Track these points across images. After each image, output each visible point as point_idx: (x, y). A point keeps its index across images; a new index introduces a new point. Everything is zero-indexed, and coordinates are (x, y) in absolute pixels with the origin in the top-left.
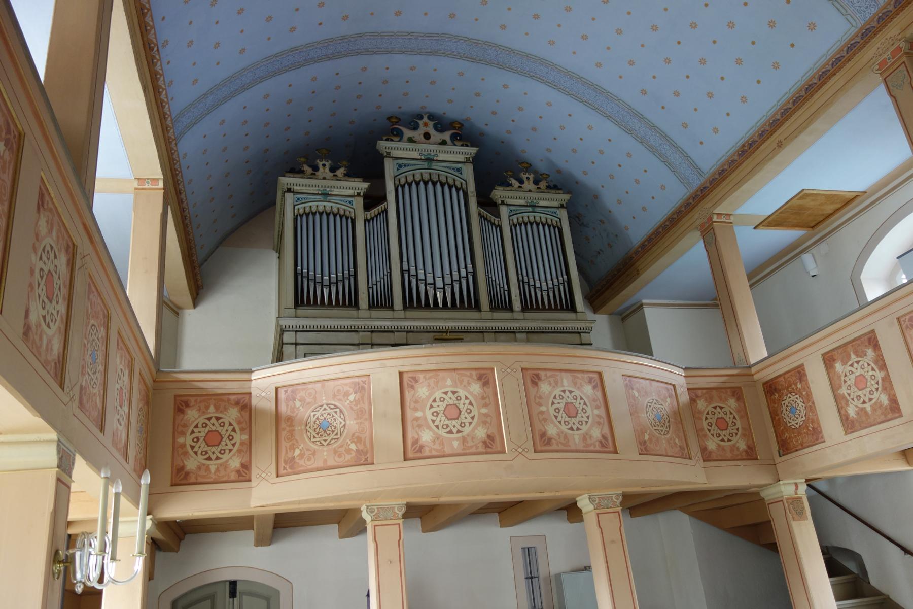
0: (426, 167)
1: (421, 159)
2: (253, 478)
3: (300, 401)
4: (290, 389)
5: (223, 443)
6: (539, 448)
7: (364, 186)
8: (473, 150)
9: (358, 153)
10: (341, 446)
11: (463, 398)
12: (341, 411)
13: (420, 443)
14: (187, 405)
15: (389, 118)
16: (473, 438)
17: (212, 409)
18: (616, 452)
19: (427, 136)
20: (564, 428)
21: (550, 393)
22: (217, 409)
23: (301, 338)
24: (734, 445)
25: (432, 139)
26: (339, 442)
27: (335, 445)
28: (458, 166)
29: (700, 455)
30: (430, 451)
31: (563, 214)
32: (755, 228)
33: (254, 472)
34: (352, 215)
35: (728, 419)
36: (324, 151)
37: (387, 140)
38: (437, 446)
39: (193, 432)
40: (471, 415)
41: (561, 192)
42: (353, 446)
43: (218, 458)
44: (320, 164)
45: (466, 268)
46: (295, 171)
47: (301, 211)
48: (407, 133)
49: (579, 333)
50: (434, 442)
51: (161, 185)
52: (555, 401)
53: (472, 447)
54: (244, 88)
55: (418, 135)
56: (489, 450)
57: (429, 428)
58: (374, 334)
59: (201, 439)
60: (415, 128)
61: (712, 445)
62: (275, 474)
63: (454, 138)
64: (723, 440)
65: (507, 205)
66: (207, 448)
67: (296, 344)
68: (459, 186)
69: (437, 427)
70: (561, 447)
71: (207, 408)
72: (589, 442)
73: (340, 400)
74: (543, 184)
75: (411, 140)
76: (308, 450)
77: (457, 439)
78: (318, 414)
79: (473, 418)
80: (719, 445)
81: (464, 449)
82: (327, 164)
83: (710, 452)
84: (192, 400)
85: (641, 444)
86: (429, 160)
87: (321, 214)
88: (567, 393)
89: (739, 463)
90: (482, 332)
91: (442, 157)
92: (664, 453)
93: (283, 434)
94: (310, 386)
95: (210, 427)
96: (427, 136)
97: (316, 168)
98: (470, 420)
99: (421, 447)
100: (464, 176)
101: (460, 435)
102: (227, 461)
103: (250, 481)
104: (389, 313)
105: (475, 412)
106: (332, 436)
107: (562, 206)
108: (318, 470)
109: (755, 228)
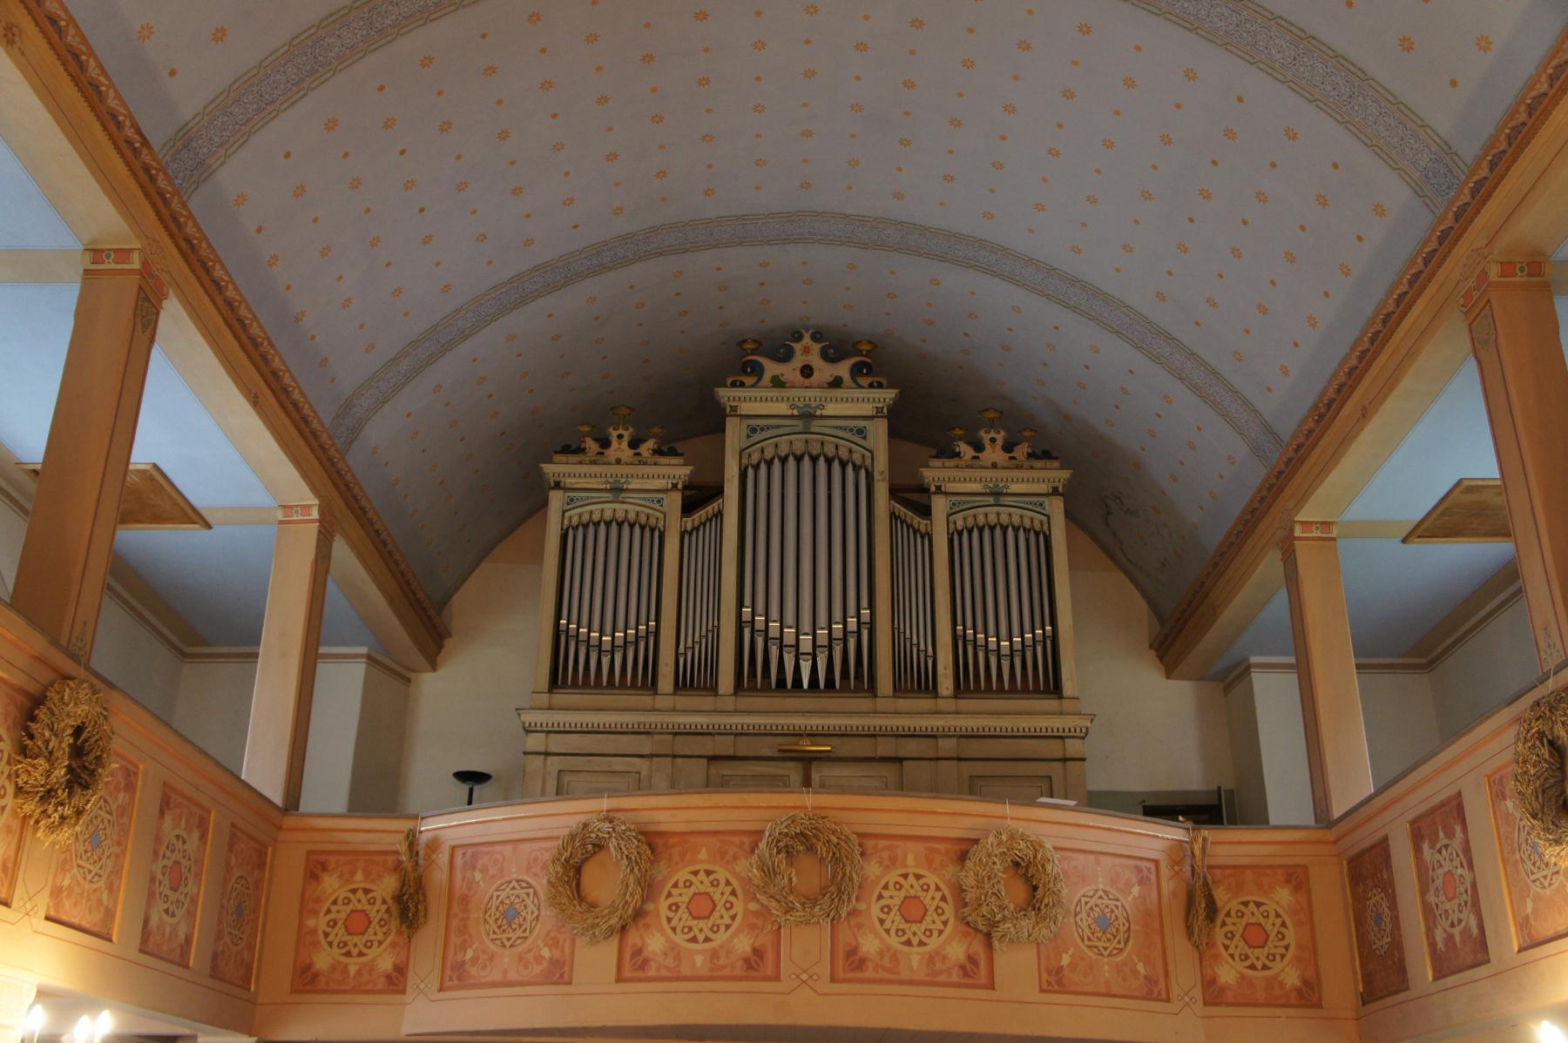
0: (800, 429)
1: (792, 417)
2: (409, 989)
3: (482, 871)
4: (470, 851)
5: (928, 919)
6: (841, 975)
7: (679, 471)
8: (889, 395)
9: (680, 409)
10: (529, 951)
11: (723, 882)
12: (535, 893)
13: (645, 954)
14: (324, 867)
15: (740, 344)
16: (728, 952)
17: (359, 876)
18: (991, 986)
19: (807, 371)
20: (894, 941)
21: (879, 878)
22: (367, 874)
23: (556, 743)
24: (1275, 977)
25: (816, 377)
26: (528, 943)
27: (520, 949)
28: (861, 423)
29: (1197, 993)
30: (658, 969)
31: (1056, 507)
32: (1404, 541)
33: (412, 979)
34: (661, 524)
35: (1268, 927)
36: (624, 411)
37: (733, 385)
38: (669, 962)
39: (329, 911)
40: (732, 912)
41: (1056, 464)
42: (546, 953)
43: (361, 954)
44: (615, 434)
45: (858, 615)
46: (571, 449)
47: (575, 521)
48: (771, 368)
49: (1062, 738)
50: (665, 954)
51: (315, 514)
52: (885, 893)
53: (724, 967)
54: (464, 336)
55: (790, 371)
56: (752, 973)
57: (663, 932)
58: (679, 738)
59: (340, 924)
60: (786, 356)
61: (1227, 974)
62: (436, 986)
63: (856, 371)
64: (1253, 967)
65: (946, 494)
66: (347, 938)
67: (547, 754)
68: (858, 463)
69: (674, 929)
70: (881, 974)
71: (352, 874)
72: (939, 966)
73: (536, 875)
74: (1021, 451)
75: (778, 383)
76: (484, 952)
77: (703, 952)
78: (503, 895)
79: (945, 923)
80: (1243, 977)
81: (711, 970)
82: (626, 434)
83: (1222, 989)
84: (332, 860)
85: (1049, 972)
86: (807, 416)
87: (608, 524)
88: (911, 879)
89: (1278, 1011)
90: (874, 736)
91: (830, 409)
92: (1103, 989)
93: (455, 922)
94: (497, 848)
95: (355, 905)
96: (807, 371)
97: (605, 443)
98: (727, 920)
99: (646, 961)
100: (870, 443)
101: (708, 946)
102: (374, 960)
103: (403, 992)
104: (706, 702)
105: (739, 907)
106: (519, 933)
107: (1055, 492)
108: (494, 985)
109: (1404, 541)
